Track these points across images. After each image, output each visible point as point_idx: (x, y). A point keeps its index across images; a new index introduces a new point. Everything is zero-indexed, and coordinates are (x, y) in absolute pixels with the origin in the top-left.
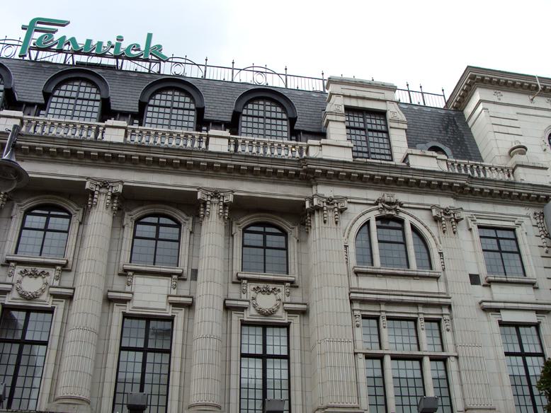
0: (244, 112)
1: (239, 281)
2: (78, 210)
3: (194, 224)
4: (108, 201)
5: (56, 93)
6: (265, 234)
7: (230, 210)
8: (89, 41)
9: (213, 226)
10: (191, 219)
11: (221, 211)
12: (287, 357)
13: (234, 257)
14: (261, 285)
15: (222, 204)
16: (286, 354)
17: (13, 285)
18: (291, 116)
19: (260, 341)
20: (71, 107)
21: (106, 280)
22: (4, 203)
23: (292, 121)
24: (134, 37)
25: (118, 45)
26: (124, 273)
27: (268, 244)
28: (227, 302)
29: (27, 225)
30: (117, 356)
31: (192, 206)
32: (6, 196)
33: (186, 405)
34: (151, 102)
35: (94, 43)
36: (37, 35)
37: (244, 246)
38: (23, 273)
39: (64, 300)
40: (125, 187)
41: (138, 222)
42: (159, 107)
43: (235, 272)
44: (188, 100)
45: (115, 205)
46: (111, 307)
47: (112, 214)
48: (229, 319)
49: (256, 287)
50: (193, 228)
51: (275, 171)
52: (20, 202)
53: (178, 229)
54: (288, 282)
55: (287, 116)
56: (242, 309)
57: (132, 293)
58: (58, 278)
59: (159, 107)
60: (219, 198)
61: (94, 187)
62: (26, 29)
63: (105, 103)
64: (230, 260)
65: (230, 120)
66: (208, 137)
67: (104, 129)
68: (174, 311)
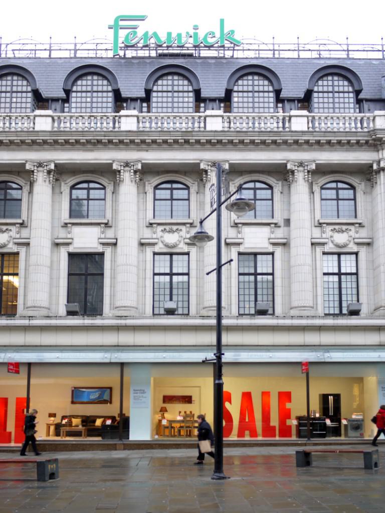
0: (236, 88)
1: (320, 225)
2: (193, 184)
3: (199, 187)
4: (45, 177)
5: (74, 89)
6: (337, 189)
7: (311, 174)
8: (169, 34)
9: (128, 187)
10: (196, 183)
11: (132, 177)
12: (356, 274)
13: (148, 208)
14: (337, 227)
15: (306, 171)
16: (187, 272)
17: (158, 239)
18: (196, 88)
19: (336, 264)
20: (170, 100)
21: (138, 232)
22: (54, 183)
23: (358, 92)
24: (208, 27)
25: (196, 34)
26: (66, 225)
27: (341, 197)
28: (227, 240)
29: (157, 197)
30: (152, 279)
31: (108, 172)
32: (55, 178)
33: (201, 306)
34: (155, 88)
35: (174, 35)
36: (123, 33)
37: (322, 199)
38: (164, 231)
39: (25, 247)
40: (317, 165)
41: (73, 187)
42: (82, 92)
43: (316, 219)
44: (105, 82)
45: (137, 179)
46: (59, 251)
47: (136, 186)
48: (229, 253)
49: (333, 228)
50: (282, 189)
51: (349, 142)
52: (149, 181)
53: (187, 191)
54: (357, 223)
55: (273, 87)
56: (154, 244)
57: (72, 239)
58: (18, 233)
59: (82, 92)
60: (304, 167)
61: (294, 167)
62: (112, 28)
63: (117, 93)
64: (313, 211)
65: (223, 95)
66: (120, 117)
67: (34, 119)
68: (18, 249)
